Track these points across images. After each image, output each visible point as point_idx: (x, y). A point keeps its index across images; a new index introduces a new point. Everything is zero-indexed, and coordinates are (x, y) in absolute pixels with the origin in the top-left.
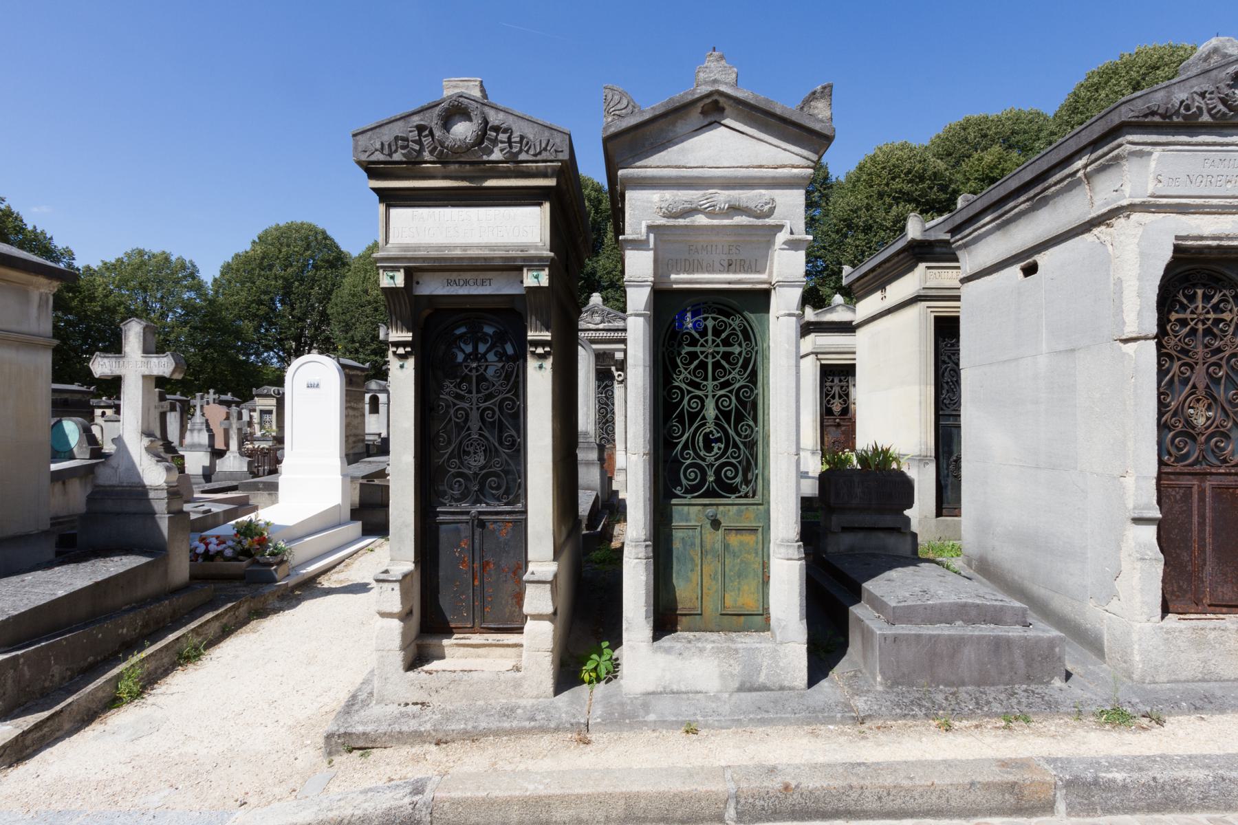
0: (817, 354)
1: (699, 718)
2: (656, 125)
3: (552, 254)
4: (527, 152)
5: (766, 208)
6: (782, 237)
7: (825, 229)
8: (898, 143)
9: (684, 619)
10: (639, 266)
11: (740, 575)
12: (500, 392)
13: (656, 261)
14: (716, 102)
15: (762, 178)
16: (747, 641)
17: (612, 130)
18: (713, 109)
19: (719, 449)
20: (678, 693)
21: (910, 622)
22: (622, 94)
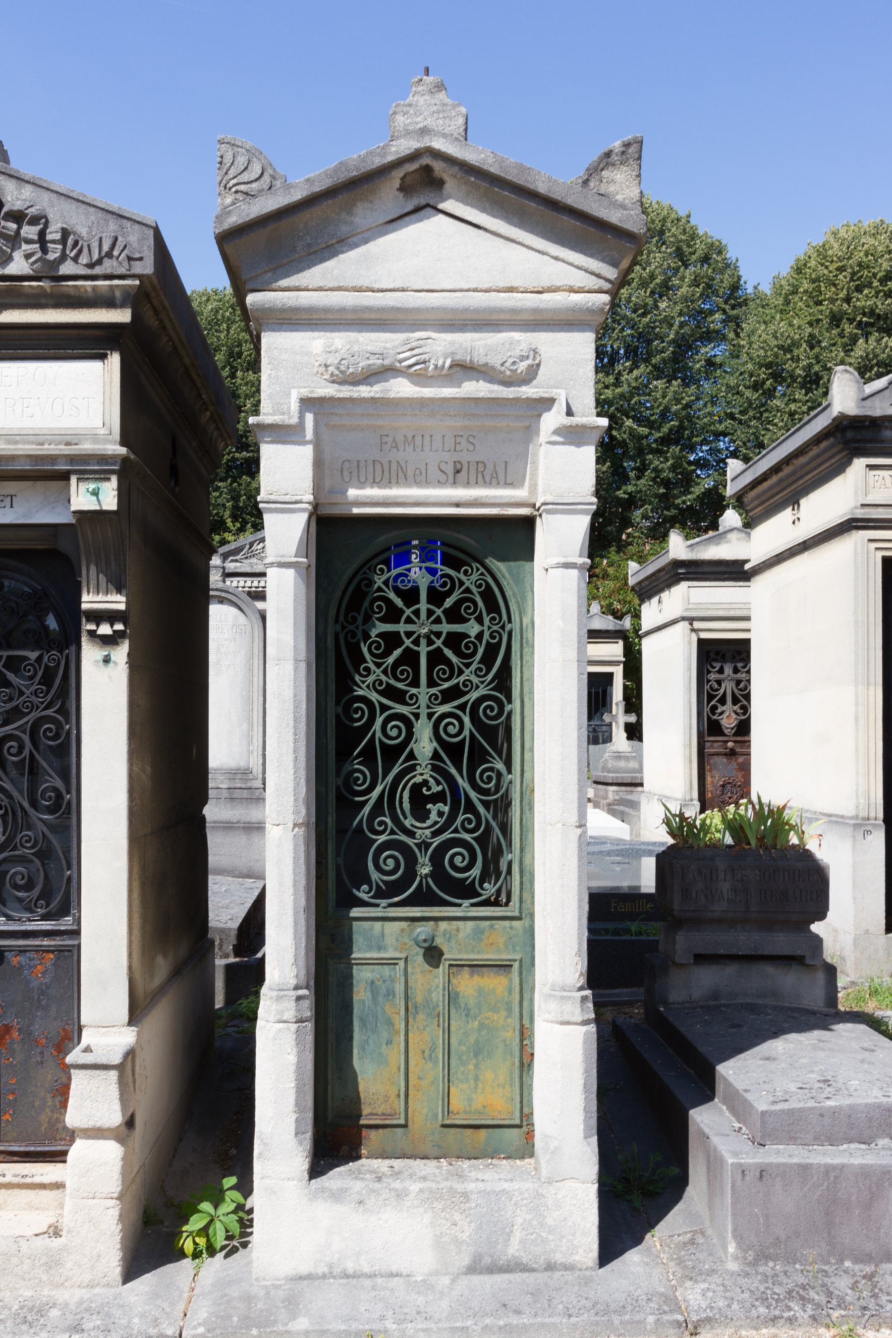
0: (691, 620)
1: (390, 1325)
2: (316, 212)
3: (123, 451)
4: (75, 259)
5: (522, 366)
6: (552, 420)
7: (733, 382)
8: (868, 223)
9: (373, 1134)
10: (285, 474)
11: (478, 1051)
12: (33, 707)
13: (318, 464)
14: (428, 169)
15: (514, 311)
16: (487, 1177)
17: (233, 220)
18: (421, 182)
19: (440, 814)
20: (356, 1276)
21: (792, 1139)
22: (253, 154)
